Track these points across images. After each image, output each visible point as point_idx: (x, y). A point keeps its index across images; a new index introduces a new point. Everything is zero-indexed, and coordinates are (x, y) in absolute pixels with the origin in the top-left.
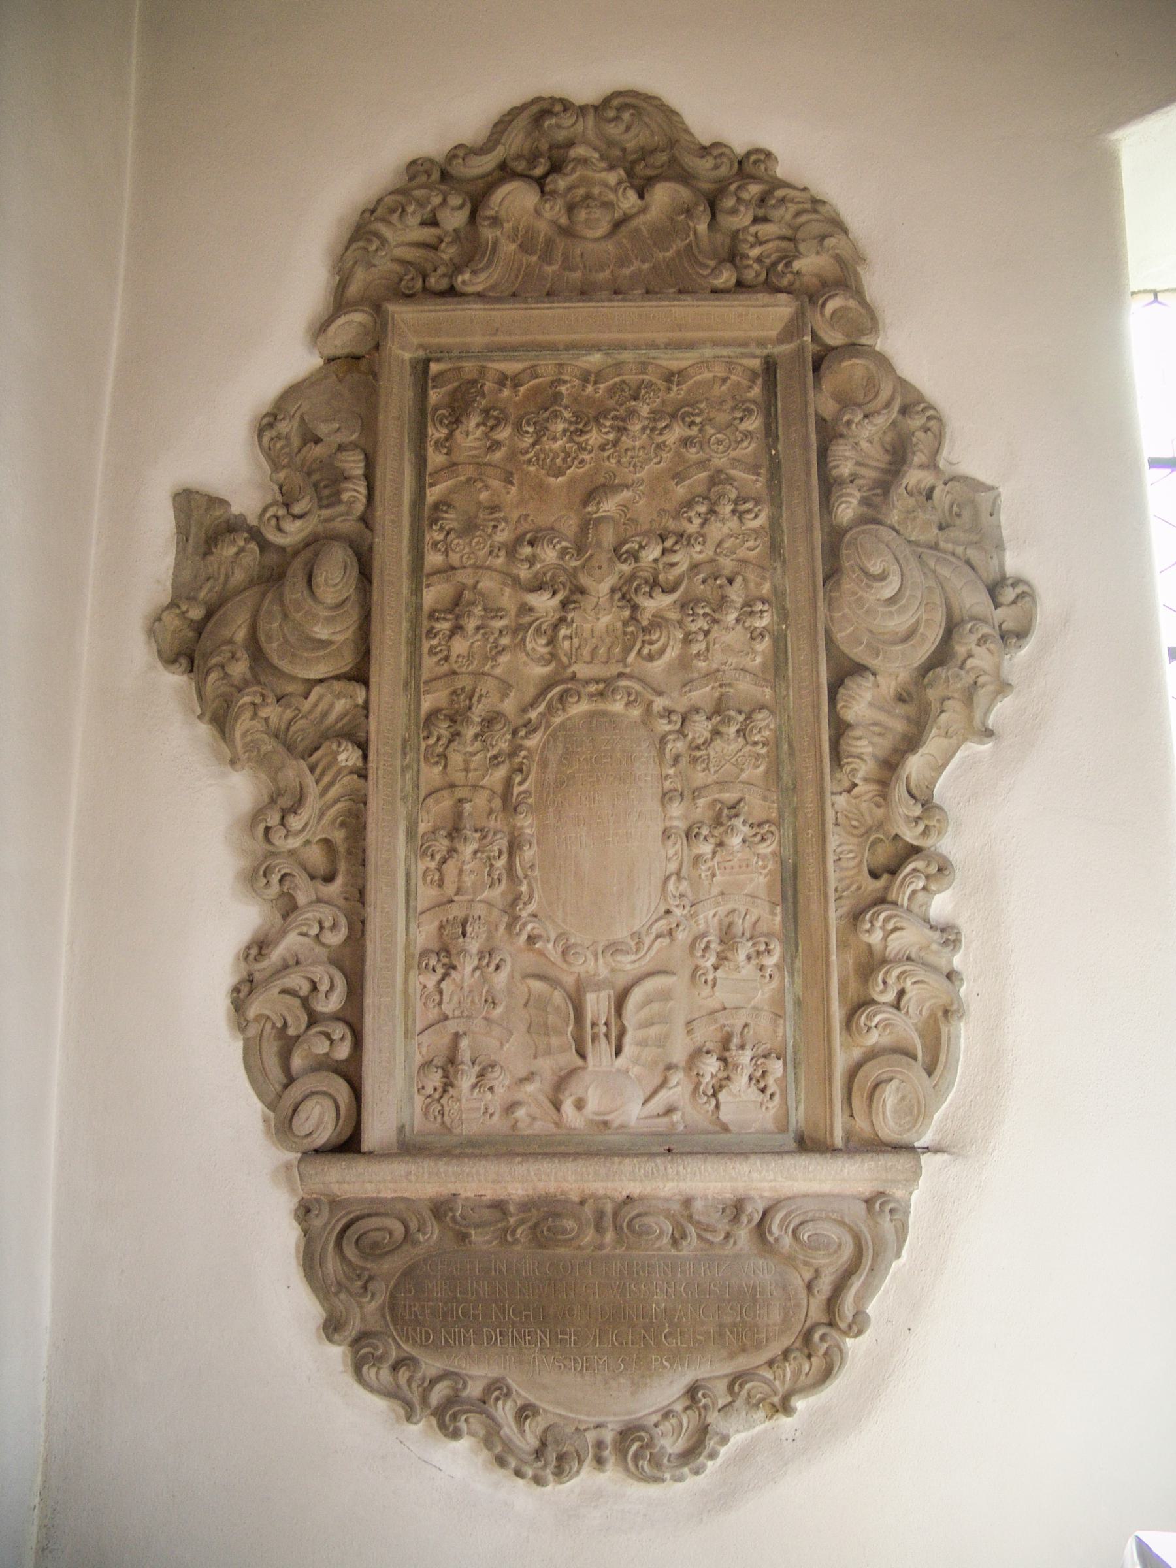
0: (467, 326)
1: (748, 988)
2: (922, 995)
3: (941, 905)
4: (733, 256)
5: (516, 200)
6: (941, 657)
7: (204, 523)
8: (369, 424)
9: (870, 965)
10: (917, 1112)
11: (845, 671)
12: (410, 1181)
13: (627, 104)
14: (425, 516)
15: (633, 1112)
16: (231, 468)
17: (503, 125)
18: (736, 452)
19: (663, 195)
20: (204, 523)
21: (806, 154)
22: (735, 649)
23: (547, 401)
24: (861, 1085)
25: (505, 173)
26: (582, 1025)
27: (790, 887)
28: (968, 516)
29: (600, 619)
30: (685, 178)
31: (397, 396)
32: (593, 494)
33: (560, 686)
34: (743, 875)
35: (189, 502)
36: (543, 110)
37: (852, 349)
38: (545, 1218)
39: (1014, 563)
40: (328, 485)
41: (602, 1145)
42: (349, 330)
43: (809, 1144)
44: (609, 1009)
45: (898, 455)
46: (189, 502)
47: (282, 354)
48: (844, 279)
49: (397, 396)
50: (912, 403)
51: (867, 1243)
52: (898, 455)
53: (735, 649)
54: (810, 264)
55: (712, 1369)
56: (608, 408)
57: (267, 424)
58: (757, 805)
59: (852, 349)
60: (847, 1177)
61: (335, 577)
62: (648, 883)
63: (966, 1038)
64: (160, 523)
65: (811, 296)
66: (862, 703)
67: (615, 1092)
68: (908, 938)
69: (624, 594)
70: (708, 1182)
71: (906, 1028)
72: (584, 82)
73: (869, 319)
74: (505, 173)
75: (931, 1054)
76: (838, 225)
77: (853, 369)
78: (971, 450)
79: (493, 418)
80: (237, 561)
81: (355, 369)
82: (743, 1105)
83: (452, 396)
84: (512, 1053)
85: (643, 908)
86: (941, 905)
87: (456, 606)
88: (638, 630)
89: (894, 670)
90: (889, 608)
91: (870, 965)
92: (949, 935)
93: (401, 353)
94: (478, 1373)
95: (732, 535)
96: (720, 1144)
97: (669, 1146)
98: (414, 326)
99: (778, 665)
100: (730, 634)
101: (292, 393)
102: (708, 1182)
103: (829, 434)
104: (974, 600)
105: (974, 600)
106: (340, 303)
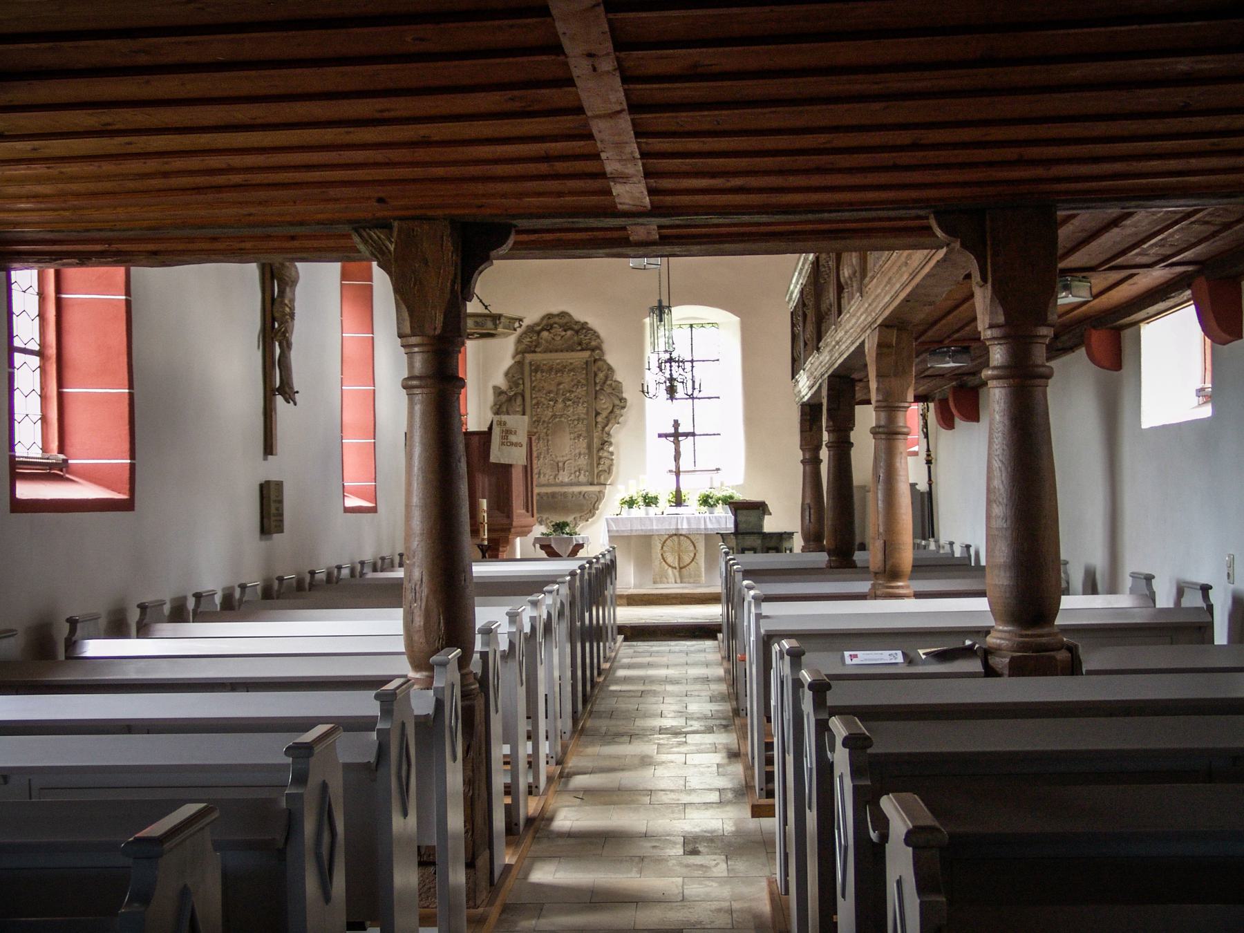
0: (538, 357)
1: (583, 461)
2: (607, 462)
3: (611, 449)
4: (580, 344)
5: (545, 334)
6: (612, 412)
7: (498, 392)
8: (523, 374)
9: (600, 458)
10: (606, 479)
11: (597, 414)
12: (727, 554)
13: (563, 314)
14: (533, 388)
15: (566, 480)
16: (500, 380)
17: (543, 318)
18: (581, 377)
19: (569, 333)
20: (498, 392)
21: (594, 322)
22: (581, 410)
23: (551, 369)
24: (599, 476)
25: (543, 329)
26: (558, 468)
27: (589, 447)
28: (617, 389)
29: (560, 405)
30: (572, 329)
31: (527, 368)
32: (559, 384)
33: (554, 416)
34: (582, 444)
35: (495, 388)
36: (549, 316)
37: (600, 359)
38: (553, 495)
39: (624, 395)
40: (517, 385)
41: (562, 484)
42: (518, 358)
43: (592, 484)
44: (408, 506)
45: (607, 377)
46: (495, 388)
47: (508, 362)
48: (599, 348)
49: (527, 368)
50: (610, 368)
51: (599, 497)
52: (607, 377)
53: (581, 410)
54: (593, 343)
55: (578, 515)
56: (561, 369)
57: (507, 374)
58: (584, 434)
59: (600, 359)
60: (596, 488)
61: (519, 400)
62: (567, 447)
63: (614, 469)
64: (490, 392)
65: (593, 350)
66: (599, 419)
67: (564, 477)
68: (606, 454)
69: (564, 401)
70: (576, 489)
71: (605, 467)
72: (555, 310)
73: (603, 353)
74: (543, 329)
75: (609, 471)
76: (598, 337)
77: (600, 363)
78: (619, 376)
79: (542, 371)
80: (503, 398)
81: (519, 364)
82: (582, 478)
83: (536, 368)
84: (548, 472)
85: (567, 451)
86: (611, 449)
87: (538, 404)
88: (566, 407)
89: (605, 414)
90: (604, 403)
91: (600, 458)
92: (612, 454)
93: (527, 361)
94: (545, 517)
95: (580, 391)
96: (579, 484)
97: (571, 484)
98: (529, 357)
99: (587, 413)
100: (580, 407)
101: (510, 368)
102: (576, 489)
103: (596, 375)
104: (617, 402)
105: (617, 402)
106: (517, 353)
